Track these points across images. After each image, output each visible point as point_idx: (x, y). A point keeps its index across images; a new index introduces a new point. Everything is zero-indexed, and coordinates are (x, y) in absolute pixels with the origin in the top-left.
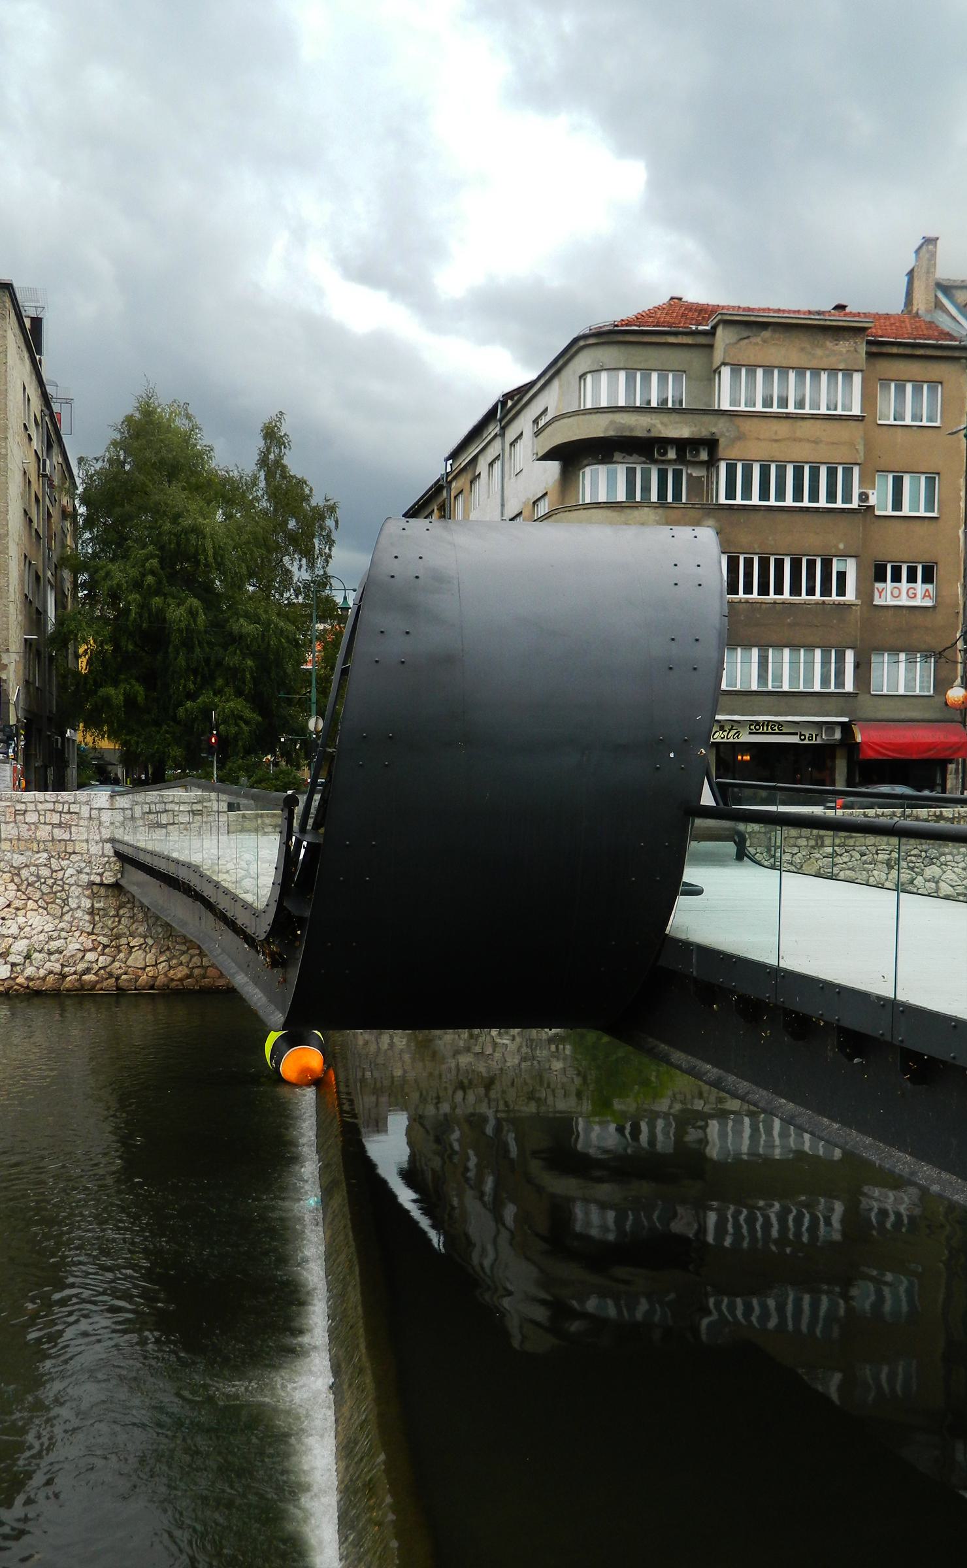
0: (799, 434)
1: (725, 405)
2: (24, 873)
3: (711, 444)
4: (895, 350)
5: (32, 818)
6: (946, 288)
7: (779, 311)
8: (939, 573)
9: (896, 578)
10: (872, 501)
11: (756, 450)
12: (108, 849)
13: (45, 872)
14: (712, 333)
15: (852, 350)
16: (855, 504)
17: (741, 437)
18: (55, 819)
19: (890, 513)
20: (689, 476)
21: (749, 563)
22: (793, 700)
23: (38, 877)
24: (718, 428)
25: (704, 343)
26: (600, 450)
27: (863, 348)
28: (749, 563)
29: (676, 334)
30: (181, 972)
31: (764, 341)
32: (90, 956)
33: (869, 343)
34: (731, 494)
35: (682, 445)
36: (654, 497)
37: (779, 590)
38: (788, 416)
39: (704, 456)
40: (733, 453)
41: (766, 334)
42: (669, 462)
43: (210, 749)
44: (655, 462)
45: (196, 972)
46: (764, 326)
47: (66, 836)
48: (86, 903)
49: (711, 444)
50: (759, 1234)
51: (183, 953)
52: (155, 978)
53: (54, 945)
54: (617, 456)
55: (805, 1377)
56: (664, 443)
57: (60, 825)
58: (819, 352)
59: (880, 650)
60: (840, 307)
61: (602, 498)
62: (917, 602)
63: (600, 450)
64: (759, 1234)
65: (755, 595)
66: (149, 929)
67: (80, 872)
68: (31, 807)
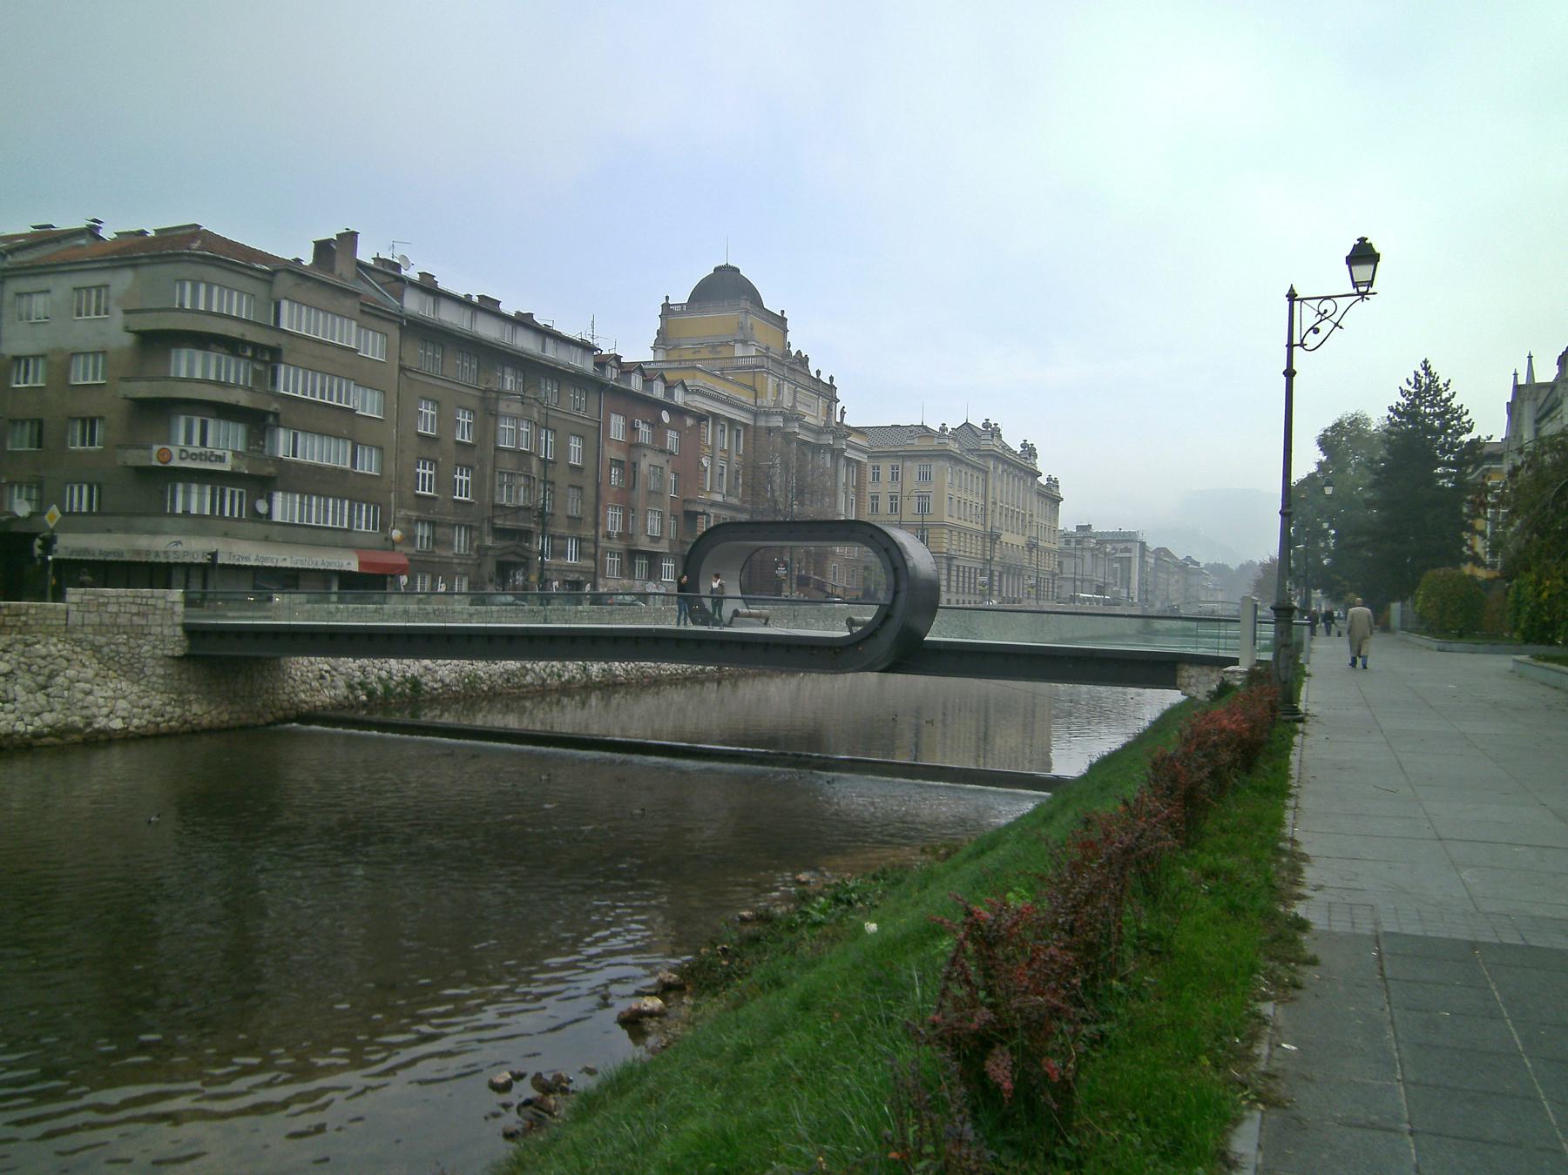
2: (106, 650)
5: (113, 608)
12: (179, 630)
13: (123, 649)
18: (134, 609)
23: (118, 653)
24: (283, 341)
25: (284, 282)
27: (358, 306)
32: (169, 709)
34: (286, 389)
35: (257, 347)
38: (320, 342)
39: (267, 358)
41: (309, 284)
43: (1469, 516)
47: (143, 622)
48: (160, 671)
50: (450, 1007)
53: (145, 701)
54: (213, 346)
55: (557, 664)
57: (138, 614)
64: (450, 1007)
67: (155, 647)
68: (113, 600)
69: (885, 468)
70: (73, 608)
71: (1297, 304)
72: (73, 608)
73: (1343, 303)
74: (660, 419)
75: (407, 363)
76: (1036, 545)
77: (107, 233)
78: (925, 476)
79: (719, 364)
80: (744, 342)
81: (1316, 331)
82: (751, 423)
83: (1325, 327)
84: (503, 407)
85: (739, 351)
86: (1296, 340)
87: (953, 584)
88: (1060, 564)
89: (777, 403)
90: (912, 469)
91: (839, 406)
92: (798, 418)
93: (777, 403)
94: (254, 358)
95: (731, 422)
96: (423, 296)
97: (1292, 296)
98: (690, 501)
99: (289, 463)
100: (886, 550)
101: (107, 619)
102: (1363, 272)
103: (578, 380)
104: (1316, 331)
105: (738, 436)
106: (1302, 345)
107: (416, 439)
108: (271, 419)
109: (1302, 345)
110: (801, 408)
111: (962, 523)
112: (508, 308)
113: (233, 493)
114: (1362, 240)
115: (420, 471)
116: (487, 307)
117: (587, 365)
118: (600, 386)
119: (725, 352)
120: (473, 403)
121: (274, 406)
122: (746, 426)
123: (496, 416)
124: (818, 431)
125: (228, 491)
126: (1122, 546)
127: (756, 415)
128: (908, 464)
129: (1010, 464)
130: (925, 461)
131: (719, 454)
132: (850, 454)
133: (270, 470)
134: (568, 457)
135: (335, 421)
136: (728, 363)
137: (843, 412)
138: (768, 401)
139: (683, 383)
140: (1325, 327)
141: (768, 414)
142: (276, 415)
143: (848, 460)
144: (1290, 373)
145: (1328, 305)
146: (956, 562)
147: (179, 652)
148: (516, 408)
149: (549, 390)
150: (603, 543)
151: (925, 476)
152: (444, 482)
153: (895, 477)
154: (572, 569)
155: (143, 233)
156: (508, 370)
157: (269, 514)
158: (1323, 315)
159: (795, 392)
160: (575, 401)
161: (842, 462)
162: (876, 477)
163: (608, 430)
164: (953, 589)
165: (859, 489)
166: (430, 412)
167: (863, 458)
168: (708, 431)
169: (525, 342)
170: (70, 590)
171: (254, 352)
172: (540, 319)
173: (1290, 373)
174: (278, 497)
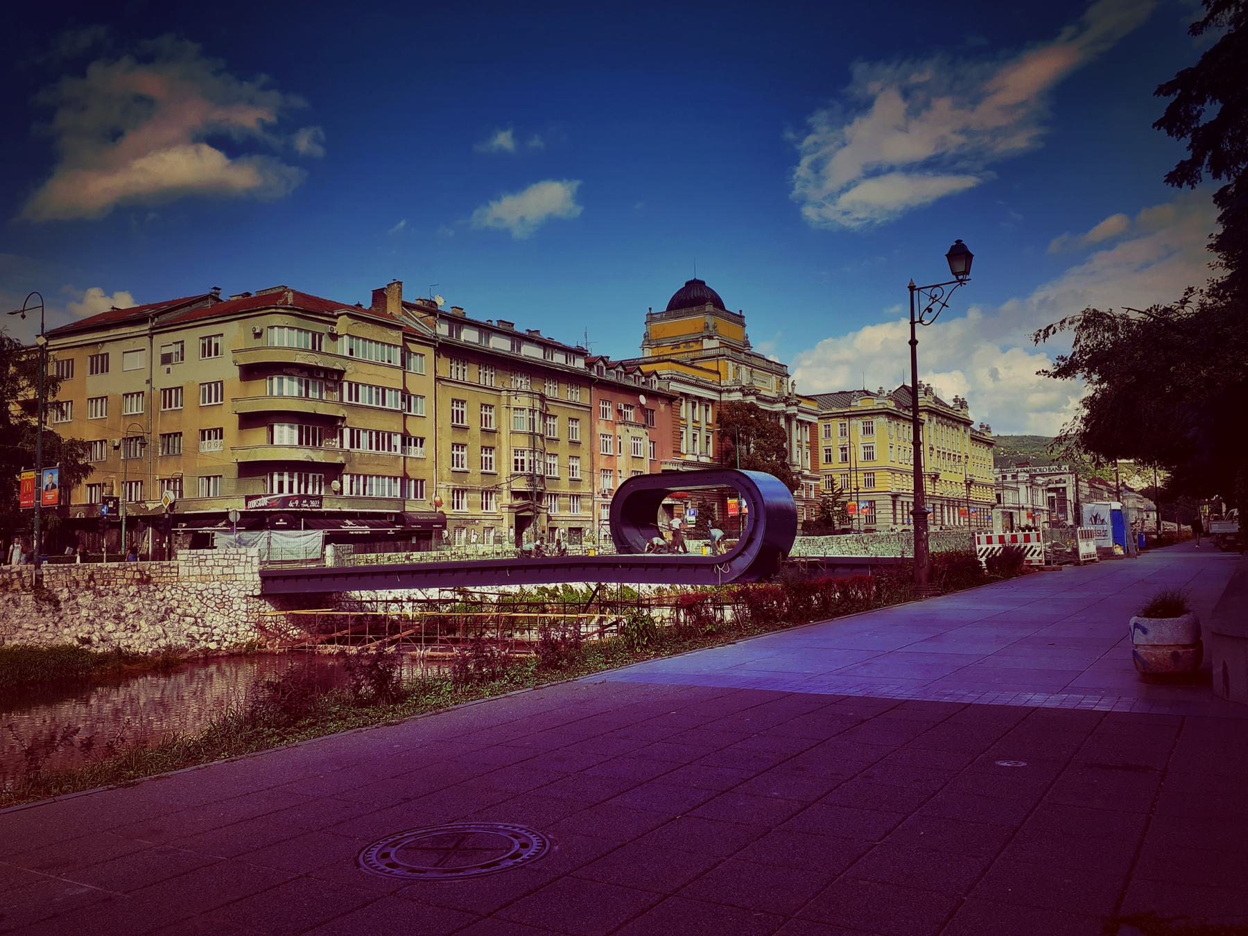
12: (257, 577)
13: (218, 592)
18: (225, 563)
34: (350, 399)
69: (835, 424)
70: (182, 563)
71: (916, 292)
72: (182, 563)
73: (948, 289)
75: (440, 374)
76: (972, 482)
77: (224, 297)
78: (868, 430)
79: (692, 355)
80: (710, 338)
81: (930, 310)
83: (936, 307)
85: (707, 344)
86: (917, 319)
87: (899, 516)
88: (998, 496)
89: (737, 381)
90: (857, 425)
91: (790, 380)
93: (737, 381)
94: (325, 379)
95: (700, 399)
97: (912, 288)
100: (748, 489)
101: (205, 571)
102: (960, 267)
104: (930, 310)
105: (707, 410)
106: (921, 321)
109: (921, 321)
110: (757, 384)
114: (959, 242)
122: (712, 401)
124: (773, 401)
125: (311, 476)
126: (1057, 478)
128: (854, 421)
129: (943, 417)
130: (868, 418)
131: (804, 445)
132: (801, 416)
136: (698, 355)
137: (793, 384)
138: (728, 381)
139: (655, 373)
140: (936, 307)
143: (801, 422)
144: (913, 343)
145: (937, 291)
146: (901, 499)
147: (257, 592)
151: (868, 430)
153: (843, 433)
155: (248, 294)
157: (341, 491)
158: (934, 299)
161: (794, 423)
162: (828, 434)
165: (813, 446)
167: (814, 419)
168: (685, 410)
170: (179, 552)
171: (326, 375)
173: (913, 343)
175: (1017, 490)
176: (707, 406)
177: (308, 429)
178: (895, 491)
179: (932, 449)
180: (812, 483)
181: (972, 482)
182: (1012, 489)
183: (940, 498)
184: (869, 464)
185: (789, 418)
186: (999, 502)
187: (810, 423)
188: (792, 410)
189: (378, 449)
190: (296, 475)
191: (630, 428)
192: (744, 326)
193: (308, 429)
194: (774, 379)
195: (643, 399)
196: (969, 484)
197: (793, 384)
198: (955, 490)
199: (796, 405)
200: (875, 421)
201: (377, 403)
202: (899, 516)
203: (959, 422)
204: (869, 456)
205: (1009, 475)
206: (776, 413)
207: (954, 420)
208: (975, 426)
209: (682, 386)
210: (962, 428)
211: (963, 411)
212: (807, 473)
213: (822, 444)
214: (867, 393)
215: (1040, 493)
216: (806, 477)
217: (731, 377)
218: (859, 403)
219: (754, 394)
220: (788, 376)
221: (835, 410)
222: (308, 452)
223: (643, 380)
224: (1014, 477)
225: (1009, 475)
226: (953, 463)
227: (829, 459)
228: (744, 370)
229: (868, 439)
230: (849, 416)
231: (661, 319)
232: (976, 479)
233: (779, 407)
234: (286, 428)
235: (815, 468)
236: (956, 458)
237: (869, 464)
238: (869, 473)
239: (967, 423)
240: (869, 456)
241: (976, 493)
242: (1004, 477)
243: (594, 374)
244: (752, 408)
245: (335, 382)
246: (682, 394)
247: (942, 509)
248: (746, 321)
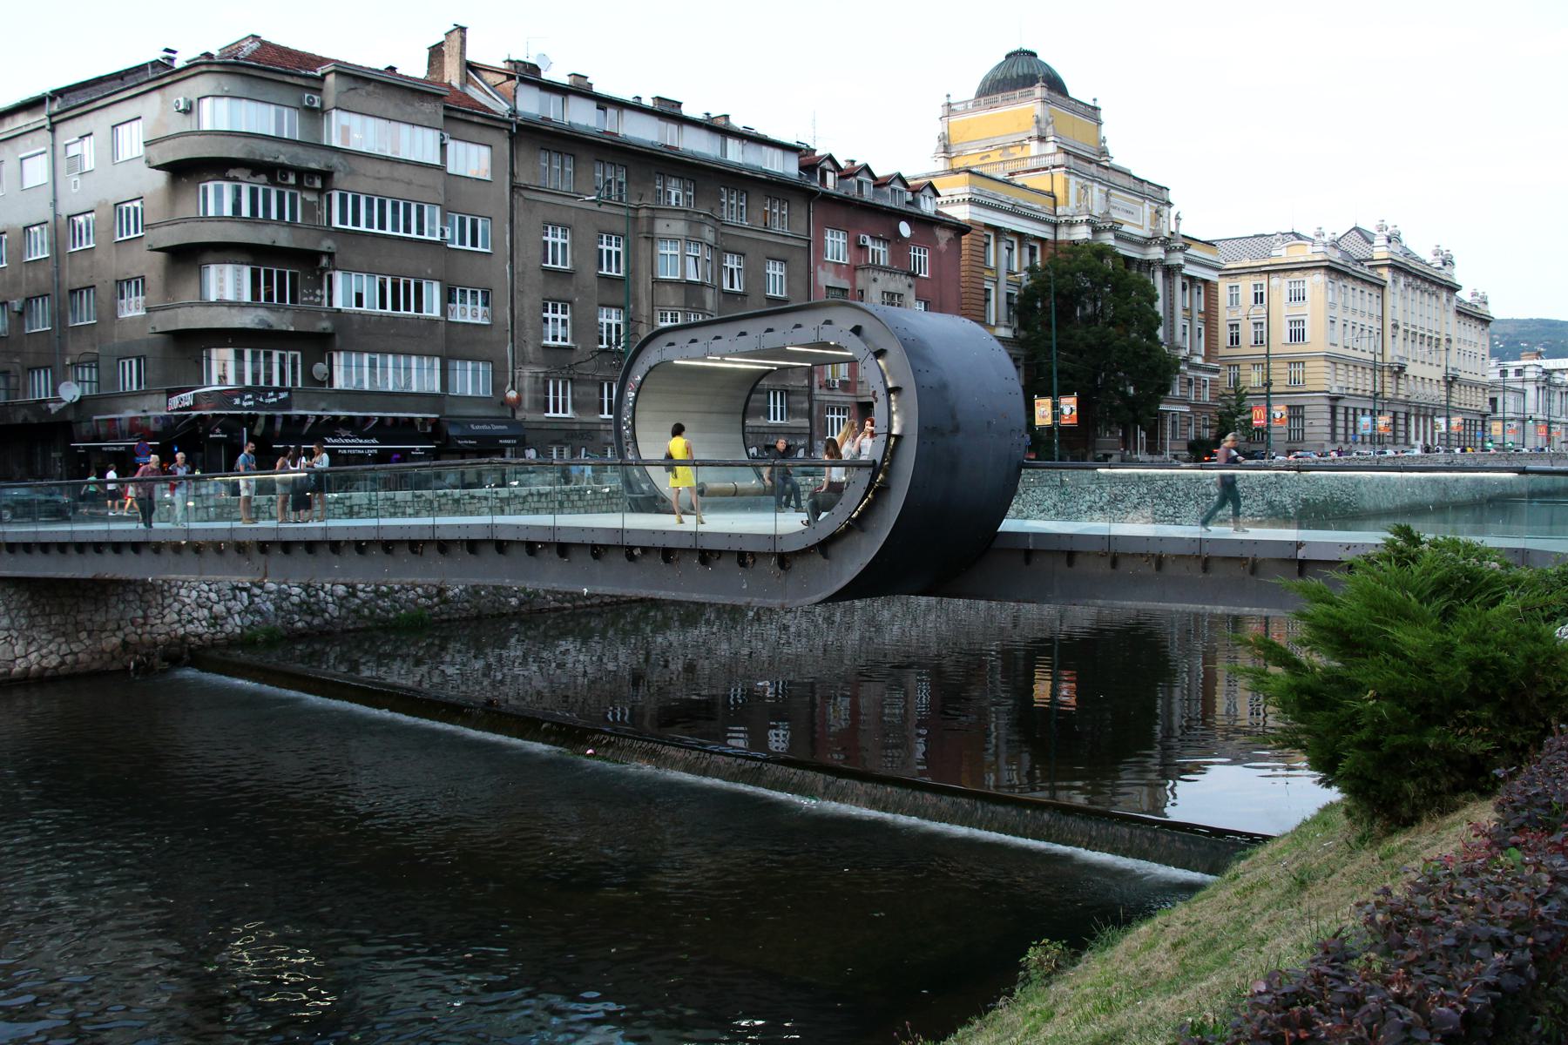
0: (396, 175)
1: (336, 143)
3: (326, 175)
4: (459, 115)
6: (471, 67)
7: (719, 128)
8: (493, 297)
9: (463, 301)
10: (448, 235)
11: (364, 185)
14: (323, 78)
15: (433, 110)
16: (438, 238)
17: (352, 173)
19: (457, 246)
20: (304, 200)
21: (407, 286)
22: (397, 399)
24: (335, 160)
26: (217, 167)
27: (441, 112)
28: (407, 286)
29: (292, 75)
30: (54, 661)
31: (368, 94)
33: (446, 108)
34: (343, 220)
35: (303, 174)
36: (274, 216)
37: (407, 308)
39: (318, 184)
40: (346, 185)
41: (370, 88)
42: (288, 186)
44: (275, 184)
45: (69, 659)
46: (368, 81)
49: (326, 175)
51: (50, 642)
52: (28, 669)
56: (285, 169)
58: (409, 109)
59: (456, 358)
60: (392, 69)
61: (211, 213)
62: (479, 321)
63: (217, 167)
65: (412, 312)
66: (12, 621)
74: (898, 233)
75: (522, 180)
79: (1011, 167)
82: (1050, 237)
84: (661, 227)
87: (1341, 431)
88: (1493, 401)
90: (1280, 286)
91: (1173, 212)
92: (1115, 228)
94: (299, 185)
95: (1021, 236)
96: (663, 124)
98: (463, 292)
99: (347, 314)
103: (773, 186)
107: (541, 276)
108: (324, 261)
110: (1116, 215)
111: (1350, 353)
112: (556, 73)
113: (282, 358)
115: (550, 315)
116: (668, 112)
117: (787, 167)
118: (809, 196)
119: (1018, 152)
120: (620, 226)
121: (326, 245)
122: (1042, 241)
123: (651, 238)
124: (1146, 243)
125: (276, 355)
127: (1056, 226)
128: (1275, 281)
129: (1416, 276)
131: (1197, 316)
132: (1189, 270)
133: (325, 325)
134: (765, 288)
135: (405, 261)
137: (1177, 218)
141: (1071, 224)
142: (331, 255)
143: (1192, 279)
146: (1342, 403)
148: (679, 227)
149: (732, 209)
150: (821, 395)
152: (584, 326)
153: (1259, 298)
154: (777, 431)
156: (674, 182)
159: (1108, 195)
160: (783, 221)
161: (1179, 281)
162: (1234, 300)
163: (821, 250)
164: (1341, 438)
165: (1210, 316)
166: (778, 273)
169: (581, 116)
172: (738, 122)
174: (339, 359)
175: (1523, 393)
176: (1032, 249)
177: (269, 275)
178: (1335, 390)
179: (1395, 326)
180: (1207, 376)
181: (1454, 378)
182: (1515, 391)
183: (1406, 403)
184: (1298, 348)
185: (1170, 271)
186: (1495, 410)
187: (1206, 282)
188: (1177, 258)
189: (396, 307)
190: (248, 353)
191: (880, 276)
192: (1099, 123)
193: (269, 275)
194: (1147, 209)
195: (905, 229)
196: (1451, 381)
197: (1177, 218)
198: (1428, 391)
199: (1182, 250)
200: (1307, 279)
201: (395, 227)
202: (1341, 431)
203: (1440, 286)
204: (1297, 335)
205: (1511, 371)
206: (1150, 264)
207: (1432, 283)
208: (1464, 295)
209: (989, 213)
210: (1444, 295)
211: (1447, 269)
212: (1199, 360)
213: (1225, 315)
214: (1298, 236)
215: (1557, 397)
216: (1197, 367)
217: (1073, 202)
218: (1283, 252)
219: (1111, 229)
220: (1169, 204)
221: (1246, 263)
222: (262, 313)
223: (909, 197)
224: (1518, 372)
225: (1511, 371)
226: (1426, 349)
227: (1235, 340)
228: (1096, 191)
229: (1297, 310)
230: (1268, 272)
231: (966, 111)
232: (1462, 375)
233: (1156, 253)
234: (229, 269)
235: (1210, 353)
236: (1433, 342)
237: (1298, 348)
238: (1297, 362)
239: (1453, 289)
240: (1297, 335)
241: (1460, 397)
242: (1504, 373)
243: (815, 184)
244: (1102, 252)
245: (320, 192)
246: (987, 226)
247: (1407, 424)
248: (1103, 116)
